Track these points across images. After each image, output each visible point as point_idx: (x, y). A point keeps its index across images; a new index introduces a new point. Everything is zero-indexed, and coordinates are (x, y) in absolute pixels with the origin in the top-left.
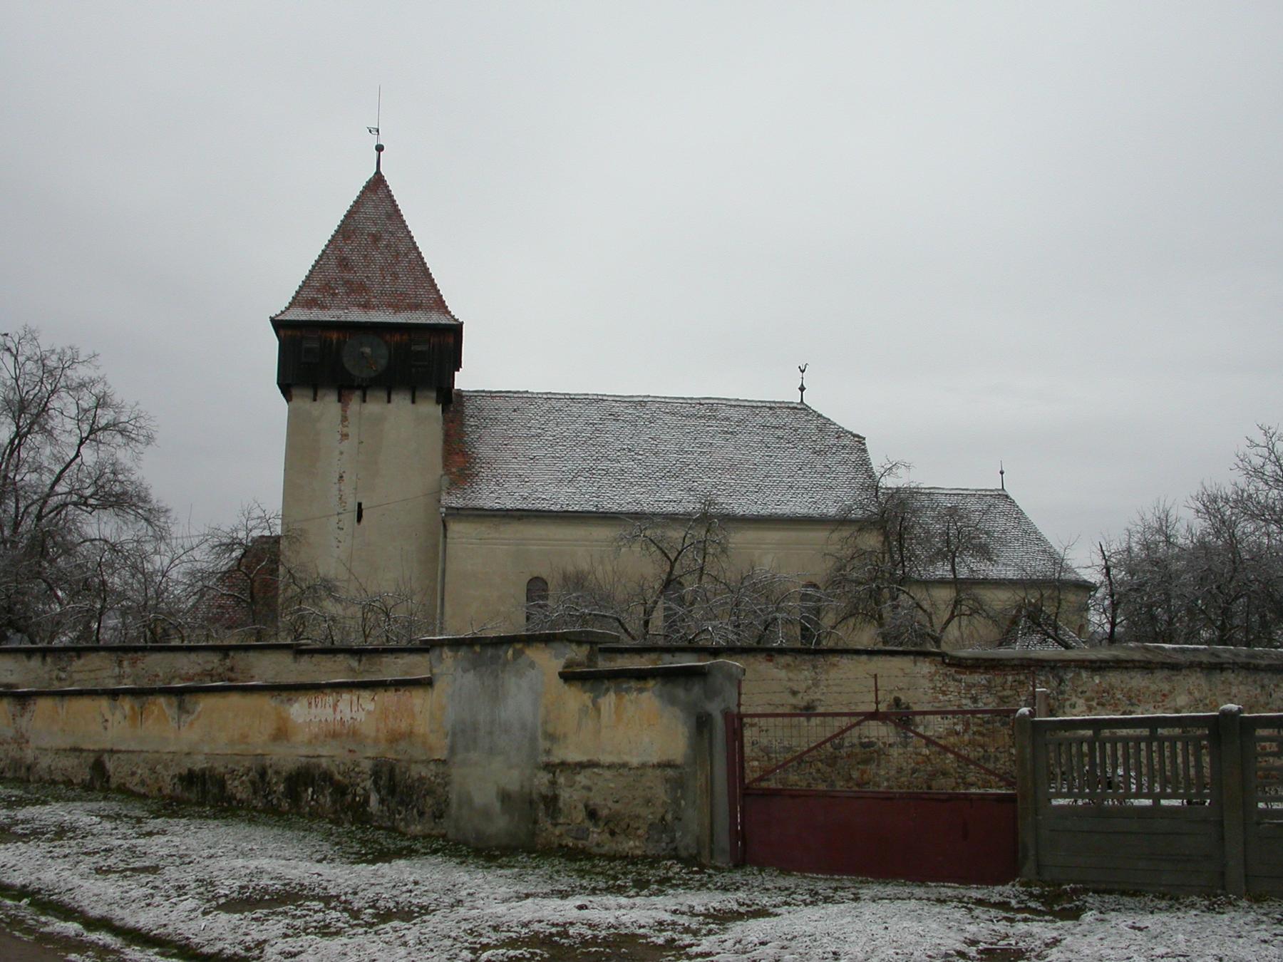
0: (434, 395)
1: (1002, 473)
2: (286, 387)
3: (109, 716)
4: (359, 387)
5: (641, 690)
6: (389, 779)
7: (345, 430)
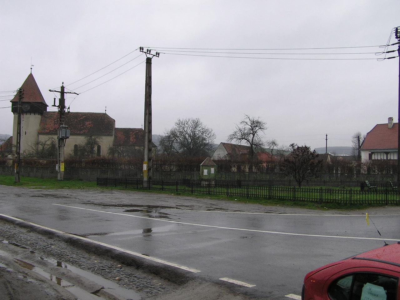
2: (14, 110)
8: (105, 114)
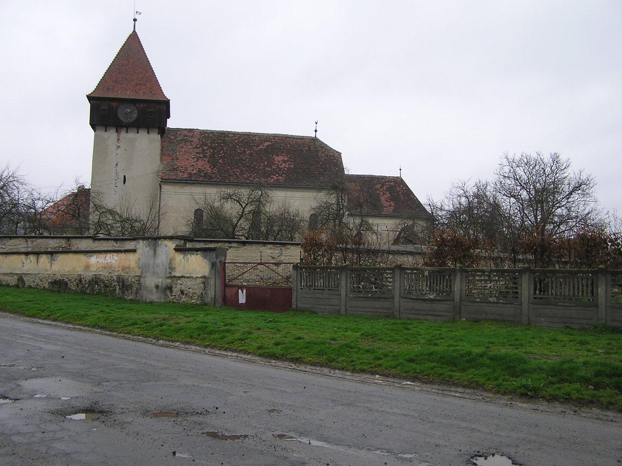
0: (157, 130)
1: (400, 170)
2: (94, 124)
3: (25, 262)
4: (125, 126)
5: (197, 254)
6: (124, 285)
7: (119, 144)
8: (315, 140)
